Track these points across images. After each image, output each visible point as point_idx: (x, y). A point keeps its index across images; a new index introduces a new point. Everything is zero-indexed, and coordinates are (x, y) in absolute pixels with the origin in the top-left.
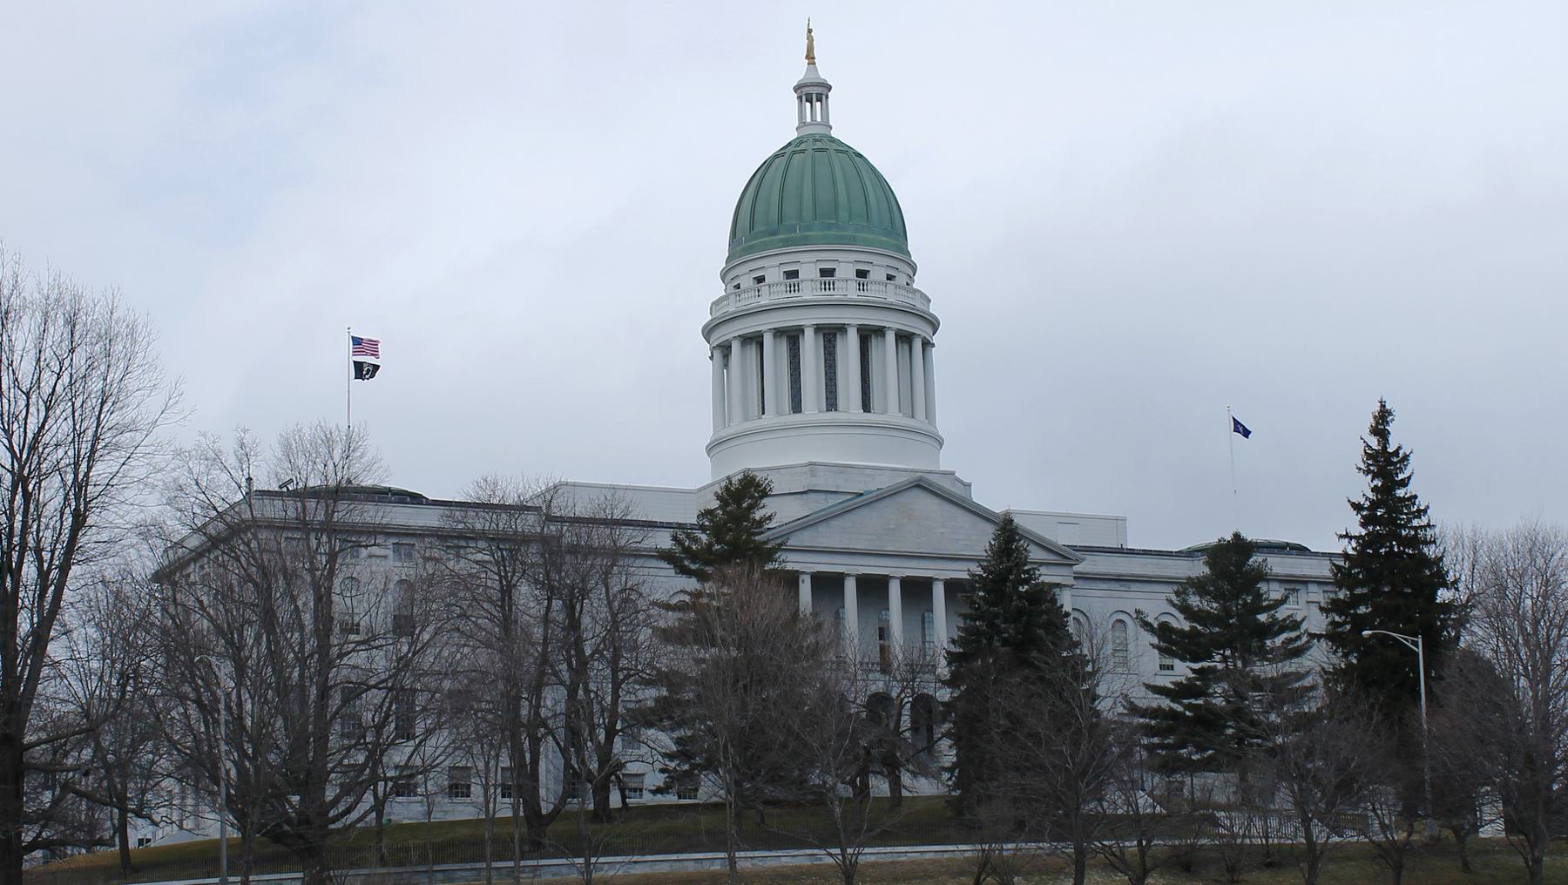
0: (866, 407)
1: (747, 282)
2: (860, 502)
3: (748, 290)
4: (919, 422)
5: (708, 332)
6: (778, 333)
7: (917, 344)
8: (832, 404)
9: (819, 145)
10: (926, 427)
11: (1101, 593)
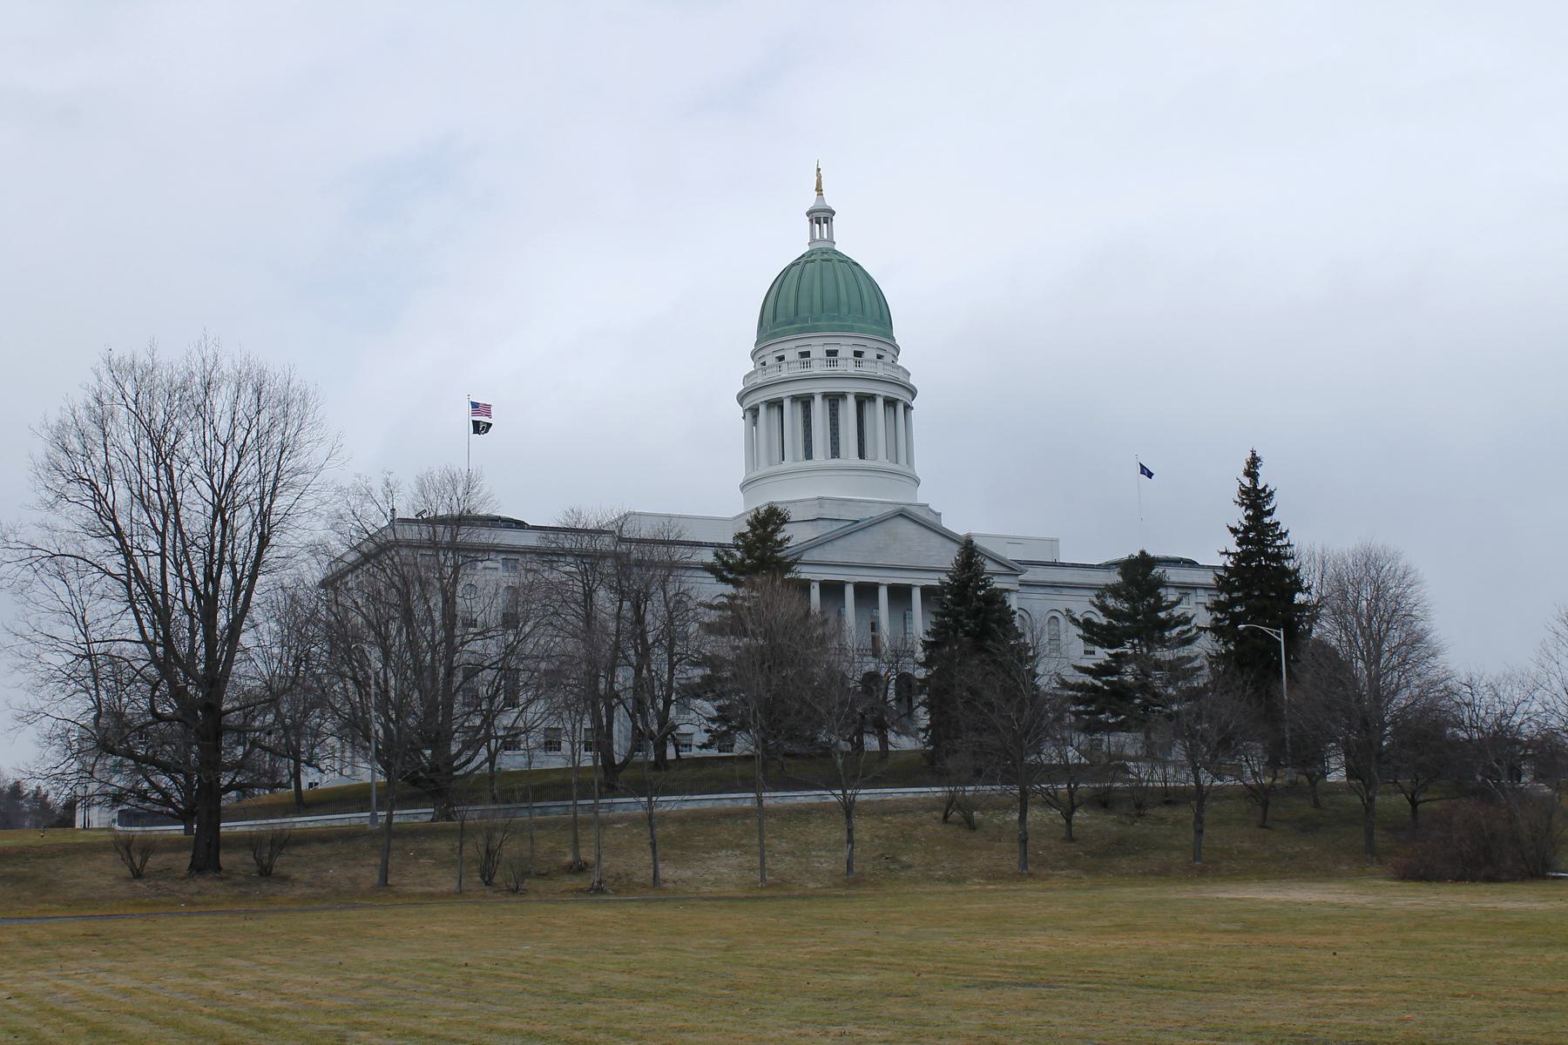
0: (861, 455)
1: (771, 360)
2: (857, 527)
6: (795, 399)
7: (900, 408)
8: (835, 453)
9: (826, 256)
10: (908, 470)
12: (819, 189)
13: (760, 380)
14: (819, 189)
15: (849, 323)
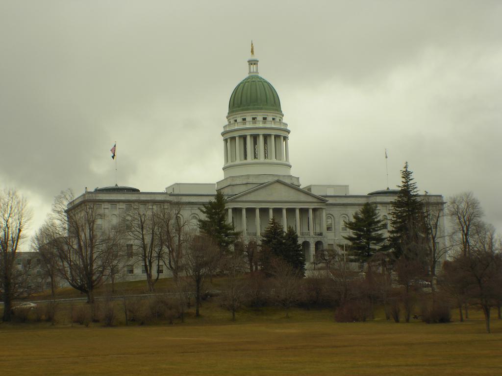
0: (255, 157)
1: (232, 121)
2: (263, 186)
3: (232, 124)
4: (284, 161)
5: (223, 134)
6: (240, 137)
9: (254, 79)
10: (287, 163)
11: (338, 209)
12: (252, 52)
13: (228, 129)
14: (252, 52)
15: (261, 106)
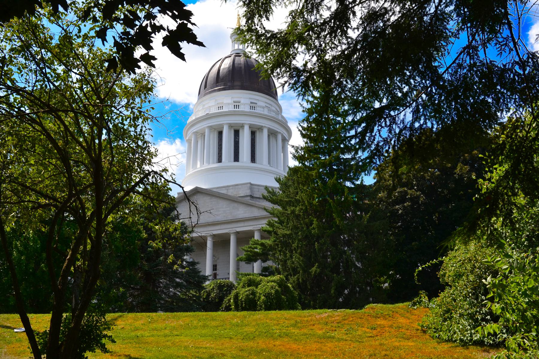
7: (280, 137)
8: (236, 158)
